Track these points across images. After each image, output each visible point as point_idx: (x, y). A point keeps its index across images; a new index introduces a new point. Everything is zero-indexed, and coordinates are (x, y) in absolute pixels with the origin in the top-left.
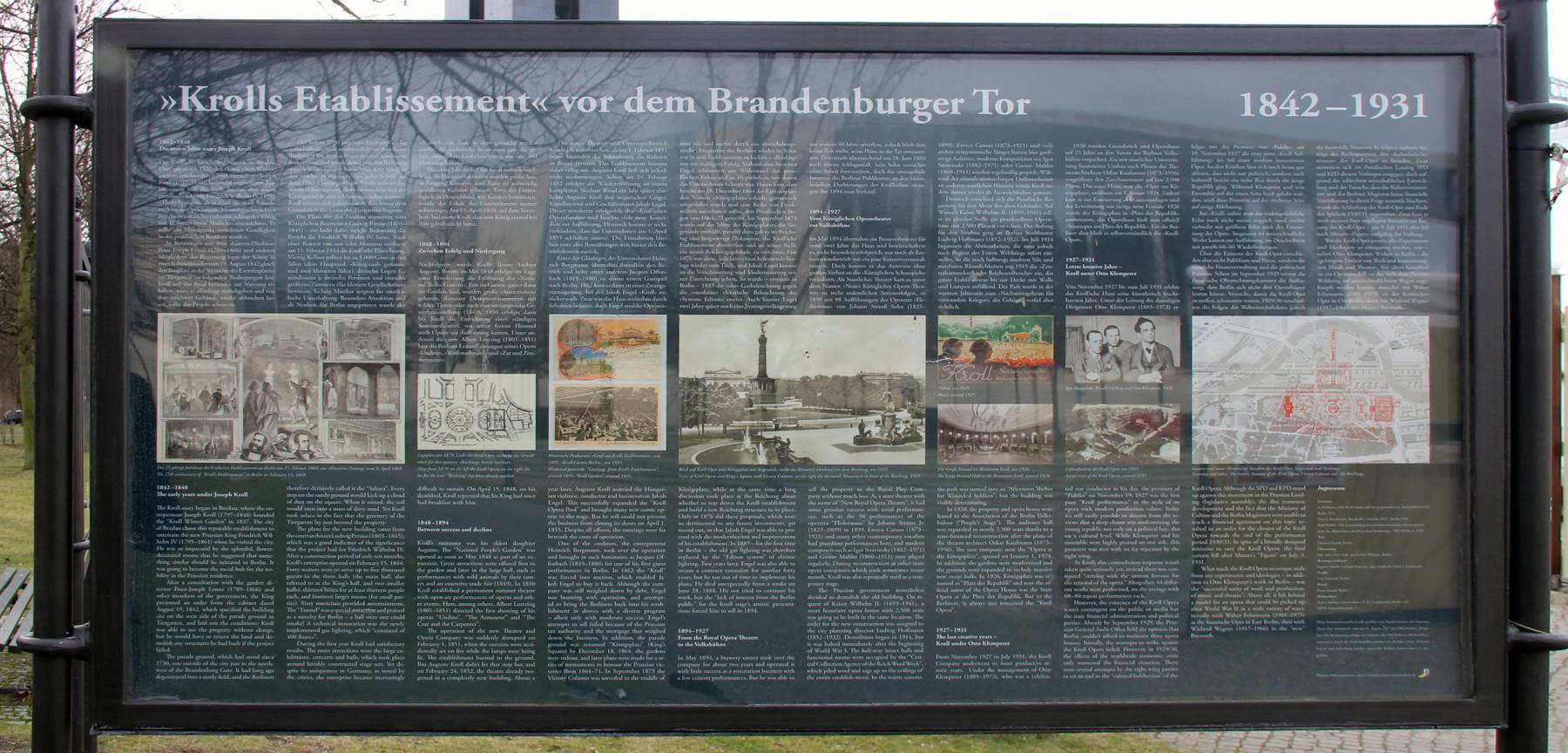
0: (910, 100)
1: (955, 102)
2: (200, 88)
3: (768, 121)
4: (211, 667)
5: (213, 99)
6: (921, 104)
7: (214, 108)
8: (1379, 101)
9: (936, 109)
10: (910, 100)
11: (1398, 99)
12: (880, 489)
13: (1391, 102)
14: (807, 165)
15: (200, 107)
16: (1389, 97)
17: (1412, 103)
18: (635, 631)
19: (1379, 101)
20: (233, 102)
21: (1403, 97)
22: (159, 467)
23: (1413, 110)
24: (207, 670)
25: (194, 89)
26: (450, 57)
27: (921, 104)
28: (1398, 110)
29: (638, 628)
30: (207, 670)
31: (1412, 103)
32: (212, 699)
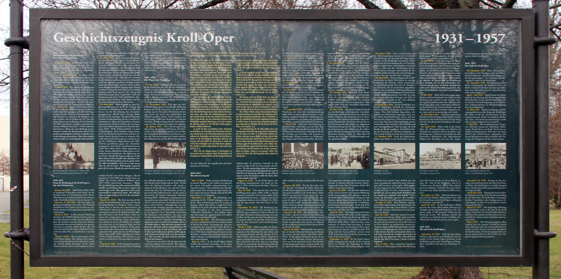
0: (181, 37)
1: (231, 38)
2: (174, 34)
3: (151, 44)
4: (79, 194)
5: (179, 38)
6: (141, 38)
7: (179, 41)
8: (445, 37)
9: (224, 41)
10: (181, 37)
11: (452, 36)
12: (225, 129)
13: (450, 37)
14: (419, 57)
15: (174, 41)
16: (449, 36)
17: (457, 37)
18: (472, 198)
19: (445, 37)
20: (186, 39)
21: (454, 35)
22: (329, 171)
23: (458, 40)
24: (78, 195)
25: (172, 34)
26: (426, 22)
27: (141, 38)
28: (452, 40)
29: (474, 197)
30: (78, 195)
31: (457, 37)
32: (462, 253)
